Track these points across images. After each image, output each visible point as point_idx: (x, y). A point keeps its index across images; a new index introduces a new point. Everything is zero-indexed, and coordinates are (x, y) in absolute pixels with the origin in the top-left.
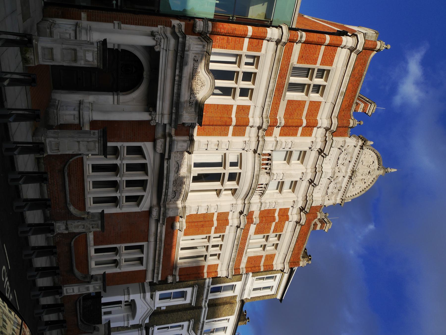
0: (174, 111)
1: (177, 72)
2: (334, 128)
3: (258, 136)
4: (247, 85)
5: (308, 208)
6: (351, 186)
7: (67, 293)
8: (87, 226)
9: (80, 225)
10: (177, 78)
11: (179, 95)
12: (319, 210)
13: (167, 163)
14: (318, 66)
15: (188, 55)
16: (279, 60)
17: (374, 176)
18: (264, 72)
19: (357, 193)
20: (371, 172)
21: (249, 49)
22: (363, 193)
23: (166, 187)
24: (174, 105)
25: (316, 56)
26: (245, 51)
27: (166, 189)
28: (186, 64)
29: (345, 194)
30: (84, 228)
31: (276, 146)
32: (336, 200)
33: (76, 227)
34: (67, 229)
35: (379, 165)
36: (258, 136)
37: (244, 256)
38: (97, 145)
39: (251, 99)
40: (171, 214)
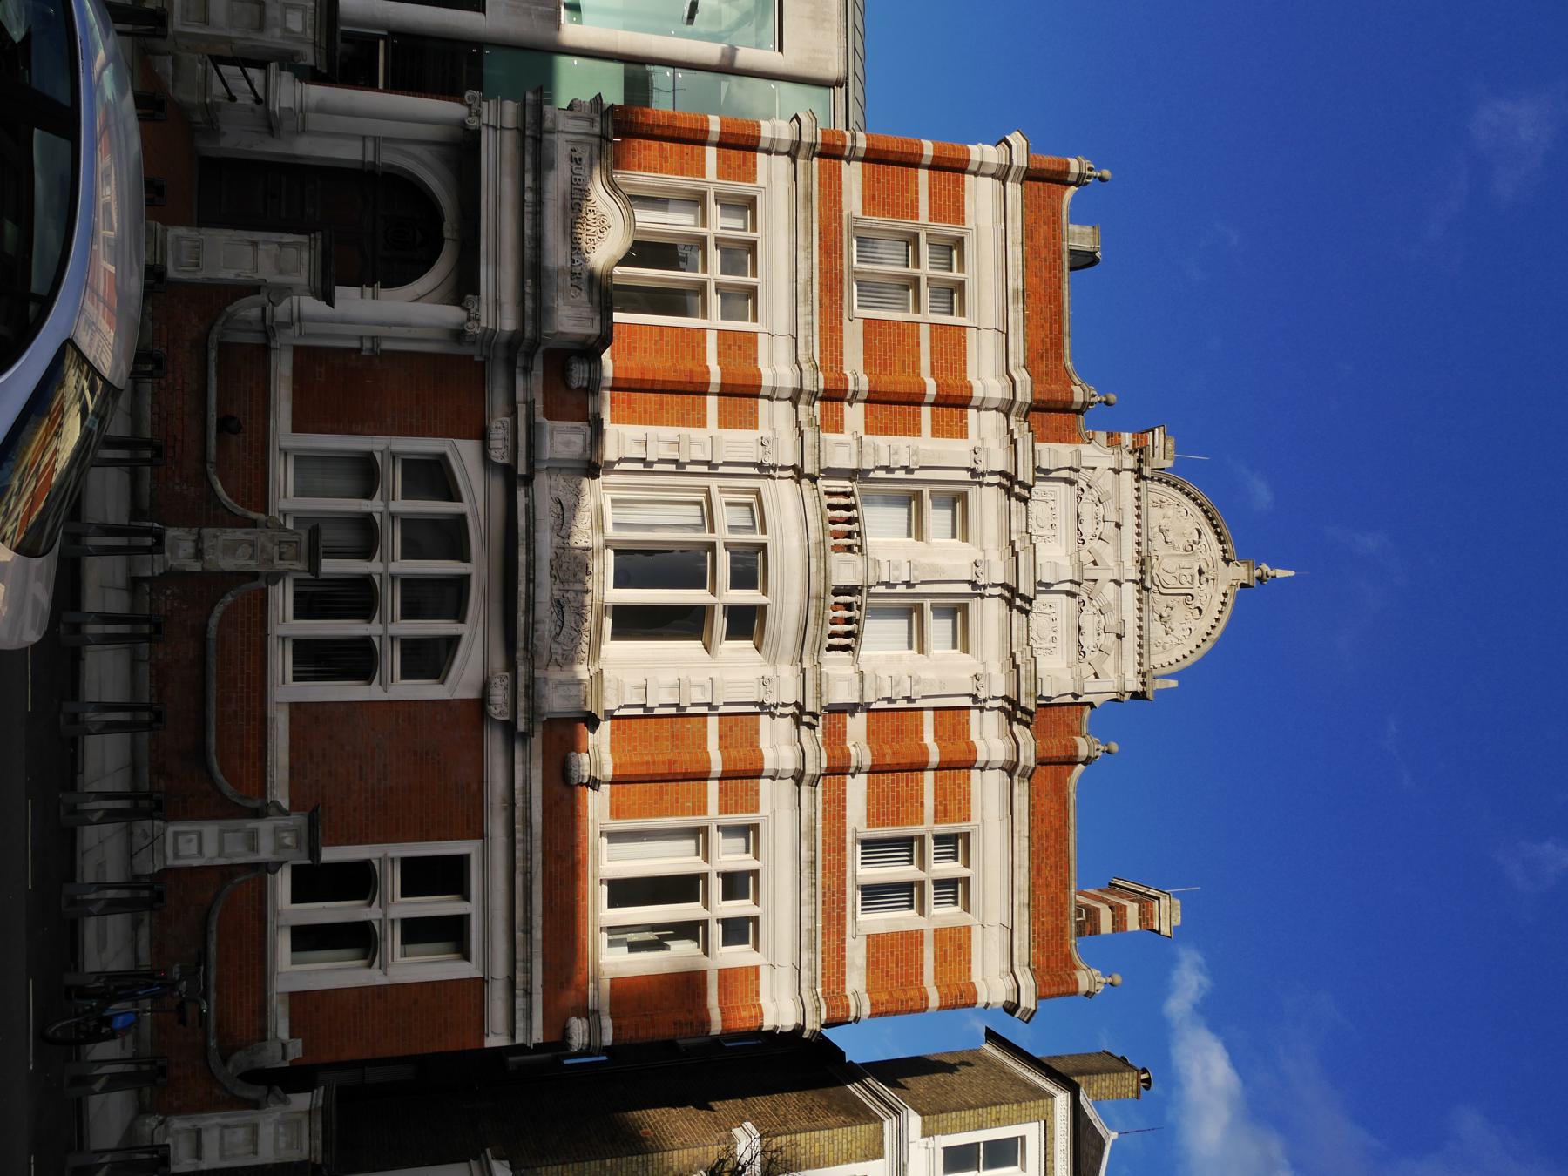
0: (527, 290)
1: (529, 181)
2: (1024, 393)
3: (798, 424)
4: (738, 908)
5: (1028, 694)
6: (1157, 629)
7: (177, 856)
8: (263, 550)
9: (243, 542)
10: (529, 196)
11: (538, 241)
12: (1076, 725)
13: (527, 495)
14: (928, 826)
15: (552, 142)
16: (808, 198)
17: (1223, 588)
19: (1187, 653)
20: (1204, 568)
21: (724, 809)
22: (1206, 647)
23: (530, 604)
24: (527, 272)
26: (713, 815)
27: (528, 581)
28: (551, 166)
30: (252, 557)
31: (860, 452)
32: (1122, 676)
33: (228, 552)
34: (199, 554)
35: (1221, 542)
36: (798, 424)
37: (849, 931)
38: (305, 255)
39: (756, 948)
40: (556, 703)
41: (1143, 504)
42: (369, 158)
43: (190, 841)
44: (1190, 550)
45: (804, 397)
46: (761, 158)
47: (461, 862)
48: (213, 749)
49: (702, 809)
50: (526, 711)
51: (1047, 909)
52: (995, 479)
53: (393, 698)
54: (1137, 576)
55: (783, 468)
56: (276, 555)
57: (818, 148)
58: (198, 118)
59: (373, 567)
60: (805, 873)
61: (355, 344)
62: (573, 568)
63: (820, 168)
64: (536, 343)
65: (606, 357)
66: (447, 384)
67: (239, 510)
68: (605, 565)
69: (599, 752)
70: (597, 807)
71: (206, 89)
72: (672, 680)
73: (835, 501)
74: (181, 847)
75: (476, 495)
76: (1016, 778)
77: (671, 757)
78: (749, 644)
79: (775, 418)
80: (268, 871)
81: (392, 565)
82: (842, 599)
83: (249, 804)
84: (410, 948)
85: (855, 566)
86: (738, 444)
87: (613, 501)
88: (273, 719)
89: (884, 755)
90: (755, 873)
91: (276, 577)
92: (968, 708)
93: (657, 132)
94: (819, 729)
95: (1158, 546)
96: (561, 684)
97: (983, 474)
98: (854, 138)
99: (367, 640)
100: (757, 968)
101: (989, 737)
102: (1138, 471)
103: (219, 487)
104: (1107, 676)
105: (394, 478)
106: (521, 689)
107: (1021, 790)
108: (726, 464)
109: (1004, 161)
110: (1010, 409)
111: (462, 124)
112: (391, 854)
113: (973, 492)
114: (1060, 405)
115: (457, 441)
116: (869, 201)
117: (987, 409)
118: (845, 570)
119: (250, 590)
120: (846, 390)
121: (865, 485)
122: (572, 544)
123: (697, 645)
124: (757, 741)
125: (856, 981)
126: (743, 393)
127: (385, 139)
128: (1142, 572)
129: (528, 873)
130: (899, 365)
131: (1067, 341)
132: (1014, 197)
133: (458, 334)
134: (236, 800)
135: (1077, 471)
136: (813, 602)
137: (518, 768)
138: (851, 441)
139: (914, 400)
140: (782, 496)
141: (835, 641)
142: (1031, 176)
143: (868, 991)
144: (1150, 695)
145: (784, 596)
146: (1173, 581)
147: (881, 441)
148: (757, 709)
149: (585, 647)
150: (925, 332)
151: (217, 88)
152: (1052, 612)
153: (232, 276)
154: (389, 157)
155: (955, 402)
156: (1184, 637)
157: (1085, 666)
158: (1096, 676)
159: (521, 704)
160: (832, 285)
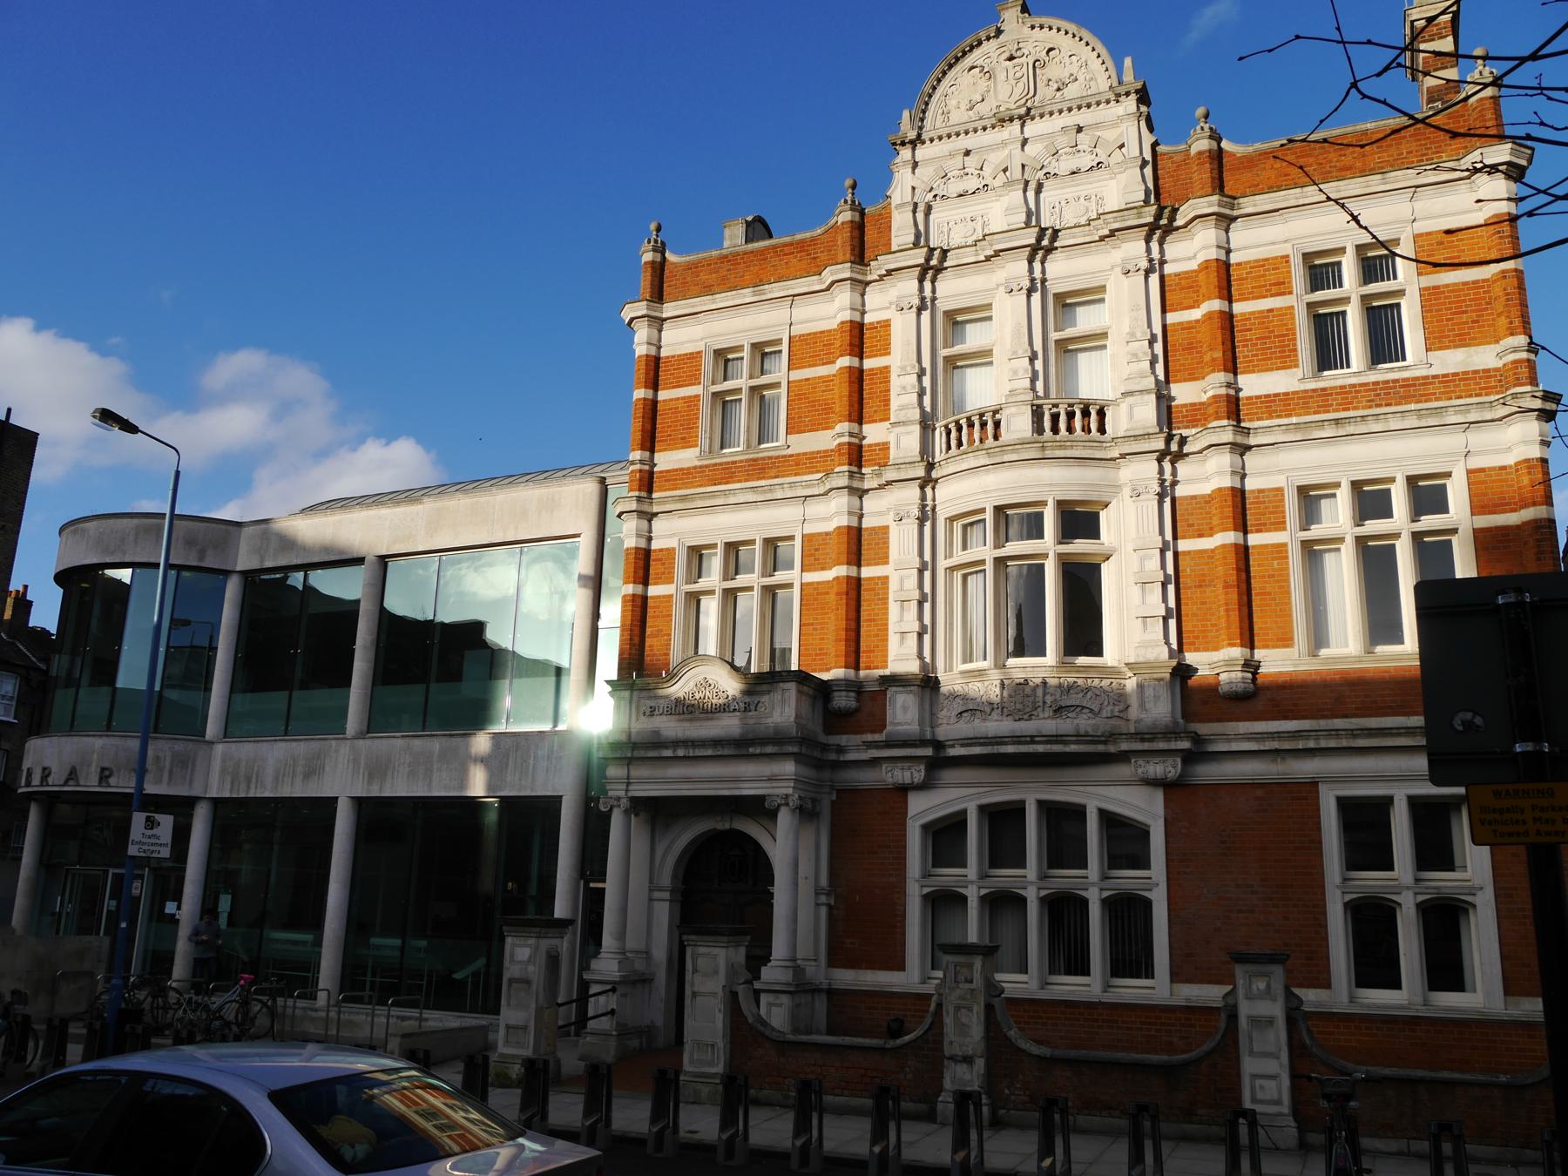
1: (668, 753)
2: (842, 271)
3: (881, 487)
4: (715, 563)
5: (1139, 215)
6: (1072, 91)
7: (1278, 1102)
9: (956, 1017)
10: (681, 753)
11: (716, 742)
13: (953, 746)
15: (638, 733)
16: (683, 498)
17: (1026, 30)
18: (1341, 459)
20: (1007, 55)
21: (1280, 525)
22: (1087, 35)
23: (1063, 741)
25: (680, 404)
26: (1288, 536)
28: (657, 733)
29: (1093, 101)
30: (970, 1009)
31: (904, 423)
33: (966, 1032)
34: (968, 1060)
35: (980, 43)
36: (881, 487)
38: (702, 950)
39: (1449, 475)
40: (1162, 710)
41: (944, 132)
42: (667, 895)
43: (1262, 1087)
44: (989, 74)
45: (856, 484)
46: (655, 545)
47: (1346, 806)
48: (1165, 1057)
49: (1280, 550)
50: (1169, 740)
51: (1393, 151)
52: (1037, 266)
53: (1164, 878)
54: (1017, 123)
55: (923, 498)
56: (968, 986)
57: (644, 494)
58: (634, 1043)
59: (1094, 898)
60: (1351, 429)
61: (823, 911)
62: (1022, 697)
63: (661, 490)
64: (805, 740)
65: (825, 676)
66: (857, 825)
67: (928, 1020)
68: (1024, 667)
69: (1217, 663)
70: (1276, 662)
71: (606, 1034)
72: (1137, 590)
73: (953, 443)
74: (1268, 1097)
75: (961, 795)
76: (1235, 213)
77: (1220, 586)
78: (1103, 515)
79: (880, 509)
80: (1298, 1009)
81: (1029, 878)
82: (1047, 424)
83: (1222, 1025)
84: (1458, 862)
85: (1013, 415)
86: (902, 543)
87: (964, 662)
88: (1188, 1000)
89: (1214, 360)
90: (1356, 485)
91: (993, 989)
92: (1162, 278)
93: (636, 640)
94: (1185, 432)
95: (985, 109)
96: (1142, 705)
97: (923, 299)
98: (633, 463)
99: (1107, 903)
100: (1469, 472)
101: (1191, 250)
102: (913, 143)
103: (907, 1038)
104: (1121, 135)
105: (948, 875)
106: (1146, 746)
107: (1248, 204)
108: (921, 554)
109: (645, 322)
110: (860, 282)
111: (627, 812)
112: (1337, 880)
113: (943, 305)
114: (856, 233)
115: (910, 814)
116: (687, 442)
117: (863, 305)
118: (1018, 424)
119: (997, 1008)
120: (850, 444)
121: (940, 414)
122: (998, 700)
123: (1105, 569)
124: (1203, 496)
125: (1485, 357)
126: (856, 543)
127: (651, 882)
128: (1011, 120)
129: (1353, 733)
130: (828, 395)
131: (798, 237)
132: (675, 308)
133: (806, 813)
134: (1218, 1037)
135: (916, 205)
136: (1048, 453)
137: (1235, 747)
138: (894, 434)
139: (857, 377)
140: (952, 495)
141: (1094, 426)
142: (658, 296)
143: (1497, 342)
144: (1139, 85)
145: (1047, 483)
146: (1021, 85)
147: (895, 403)
148: (1168, 500)
149: (1105, 683)
150: (797, 375)
151: (604, 1024)
152: (1062, 205)
153: (721, 1016)
154: (666, 879)
155: (858, 337)
156: (1078, 60)
157: (1112, 160)
158: (1122, 146)
159: (1162, 745)
160: (759, 469)
